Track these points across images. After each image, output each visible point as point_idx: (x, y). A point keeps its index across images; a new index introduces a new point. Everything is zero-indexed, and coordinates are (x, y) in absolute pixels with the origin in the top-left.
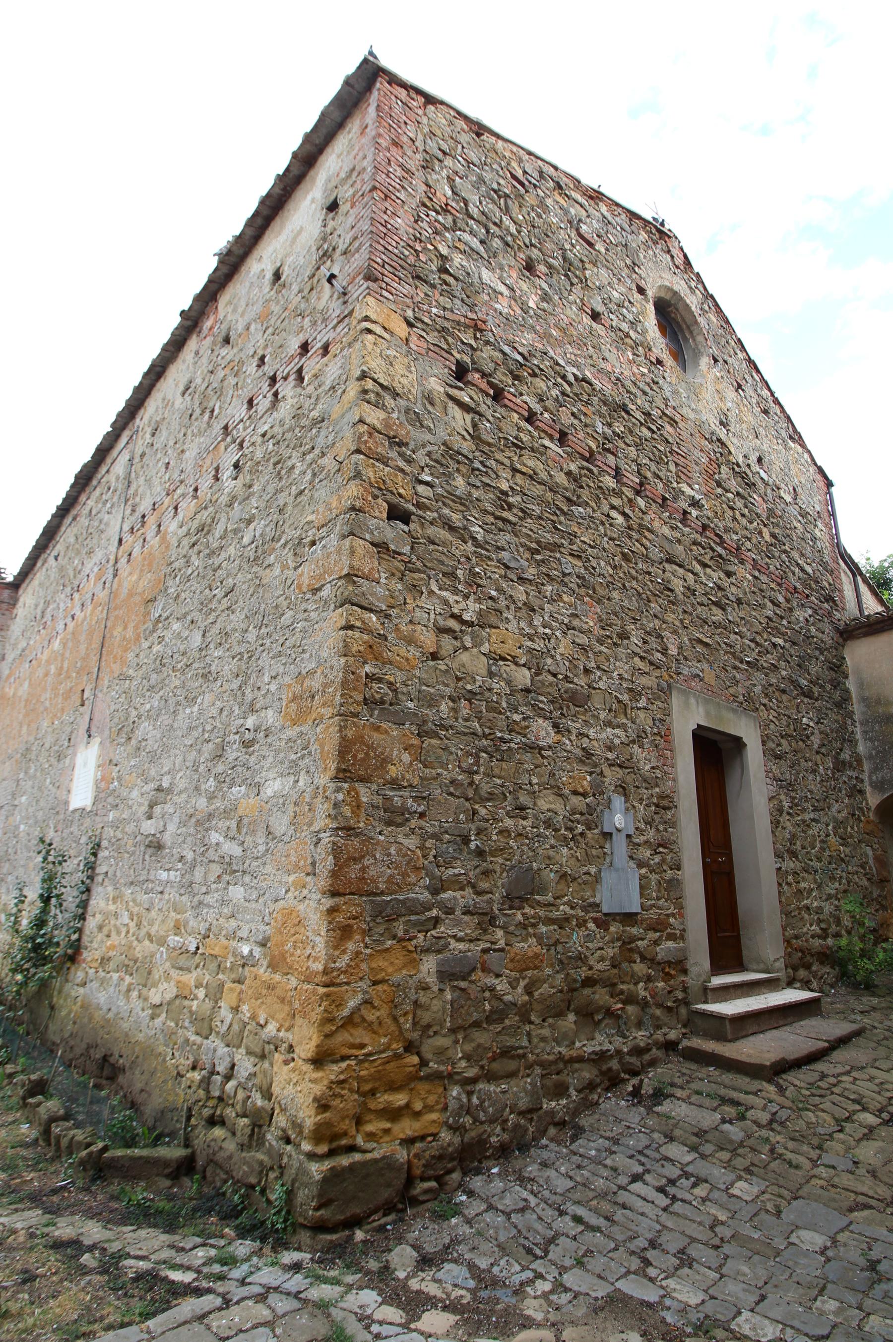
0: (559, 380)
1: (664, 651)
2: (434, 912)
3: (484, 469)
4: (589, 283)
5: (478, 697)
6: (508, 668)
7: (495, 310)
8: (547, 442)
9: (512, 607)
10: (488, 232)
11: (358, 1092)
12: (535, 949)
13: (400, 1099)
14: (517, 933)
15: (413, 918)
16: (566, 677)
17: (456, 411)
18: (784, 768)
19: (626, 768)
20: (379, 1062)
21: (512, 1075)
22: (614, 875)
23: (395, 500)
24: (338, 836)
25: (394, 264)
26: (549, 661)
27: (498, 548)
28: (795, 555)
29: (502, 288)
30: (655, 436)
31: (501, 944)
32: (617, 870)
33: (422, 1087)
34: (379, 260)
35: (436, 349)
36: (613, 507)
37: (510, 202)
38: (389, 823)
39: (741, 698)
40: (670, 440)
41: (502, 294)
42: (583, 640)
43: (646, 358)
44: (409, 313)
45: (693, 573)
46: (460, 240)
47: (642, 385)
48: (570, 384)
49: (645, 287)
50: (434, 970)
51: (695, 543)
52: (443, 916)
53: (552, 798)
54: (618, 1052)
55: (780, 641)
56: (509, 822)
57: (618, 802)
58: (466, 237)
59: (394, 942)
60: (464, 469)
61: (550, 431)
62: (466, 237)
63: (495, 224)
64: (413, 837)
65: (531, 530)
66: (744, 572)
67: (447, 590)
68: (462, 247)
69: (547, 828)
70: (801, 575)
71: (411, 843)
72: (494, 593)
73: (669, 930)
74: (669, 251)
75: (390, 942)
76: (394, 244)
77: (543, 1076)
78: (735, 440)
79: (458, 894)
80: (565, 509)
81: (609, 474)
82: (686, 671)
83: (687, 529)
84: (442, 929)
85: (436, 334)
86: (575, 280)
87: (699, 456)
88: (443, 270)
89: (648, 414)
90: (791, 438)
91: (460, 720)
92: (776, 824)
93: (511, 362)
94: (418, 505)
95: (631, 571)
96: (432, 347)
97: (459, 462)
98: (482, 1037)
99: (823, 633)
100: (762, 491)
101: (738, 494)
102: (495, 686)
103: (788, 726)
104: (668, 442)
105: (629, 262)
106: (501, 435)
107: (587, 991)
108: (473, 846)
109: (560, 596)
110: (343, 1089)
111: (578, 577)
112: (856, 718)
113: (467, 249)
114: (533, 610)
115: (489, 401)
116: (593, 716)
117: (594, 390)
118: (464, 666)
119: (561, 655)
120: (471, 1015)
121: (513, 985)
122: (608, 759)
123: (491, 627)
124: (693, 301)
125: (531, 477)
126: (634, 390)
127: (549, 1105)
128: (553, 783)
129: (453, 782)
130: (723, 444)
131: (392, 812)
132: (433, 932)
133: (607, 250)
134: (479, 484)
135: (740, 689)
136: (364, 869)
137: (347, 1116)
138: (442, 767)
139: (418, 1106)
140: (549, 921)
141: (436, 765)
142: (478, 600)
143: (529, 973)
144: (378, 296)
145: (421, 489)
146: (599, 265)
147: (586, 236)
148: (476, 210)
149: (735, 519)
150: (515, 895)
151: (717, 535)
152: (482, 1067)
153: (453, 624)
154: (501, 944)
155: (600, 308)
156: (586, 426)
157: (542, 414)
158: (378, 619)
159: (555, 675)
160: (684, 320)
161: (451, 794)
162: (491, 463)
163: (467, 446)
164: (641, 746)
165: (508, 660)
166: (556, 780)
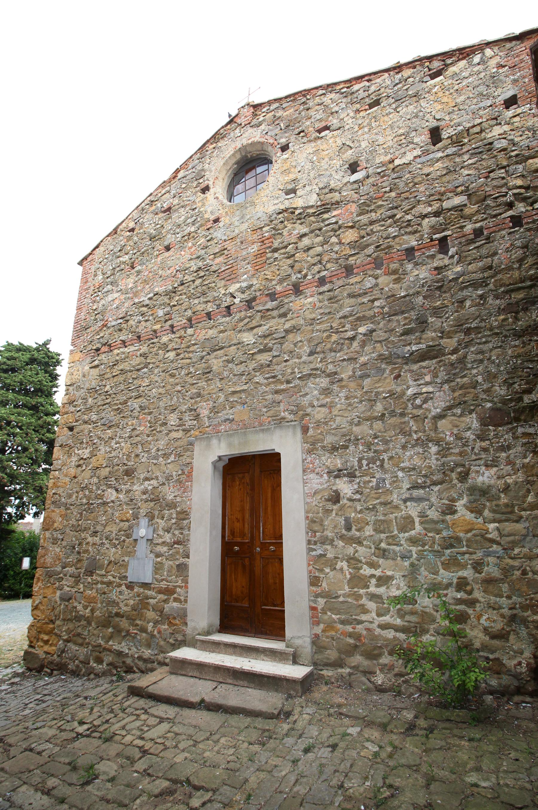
22: (136, 561)
31: (82, 590)
32: (138, 559)
38: (53, 544)
57: (144, 522)
71: (58, 550)
73: (175, 596)
79: (70, 569)
98: (71, 626)
107: (117, 619)
121: (85, 607)
127: (93, 664)
136: (45, 560)
140: (103, 583)
160: (259, 151)
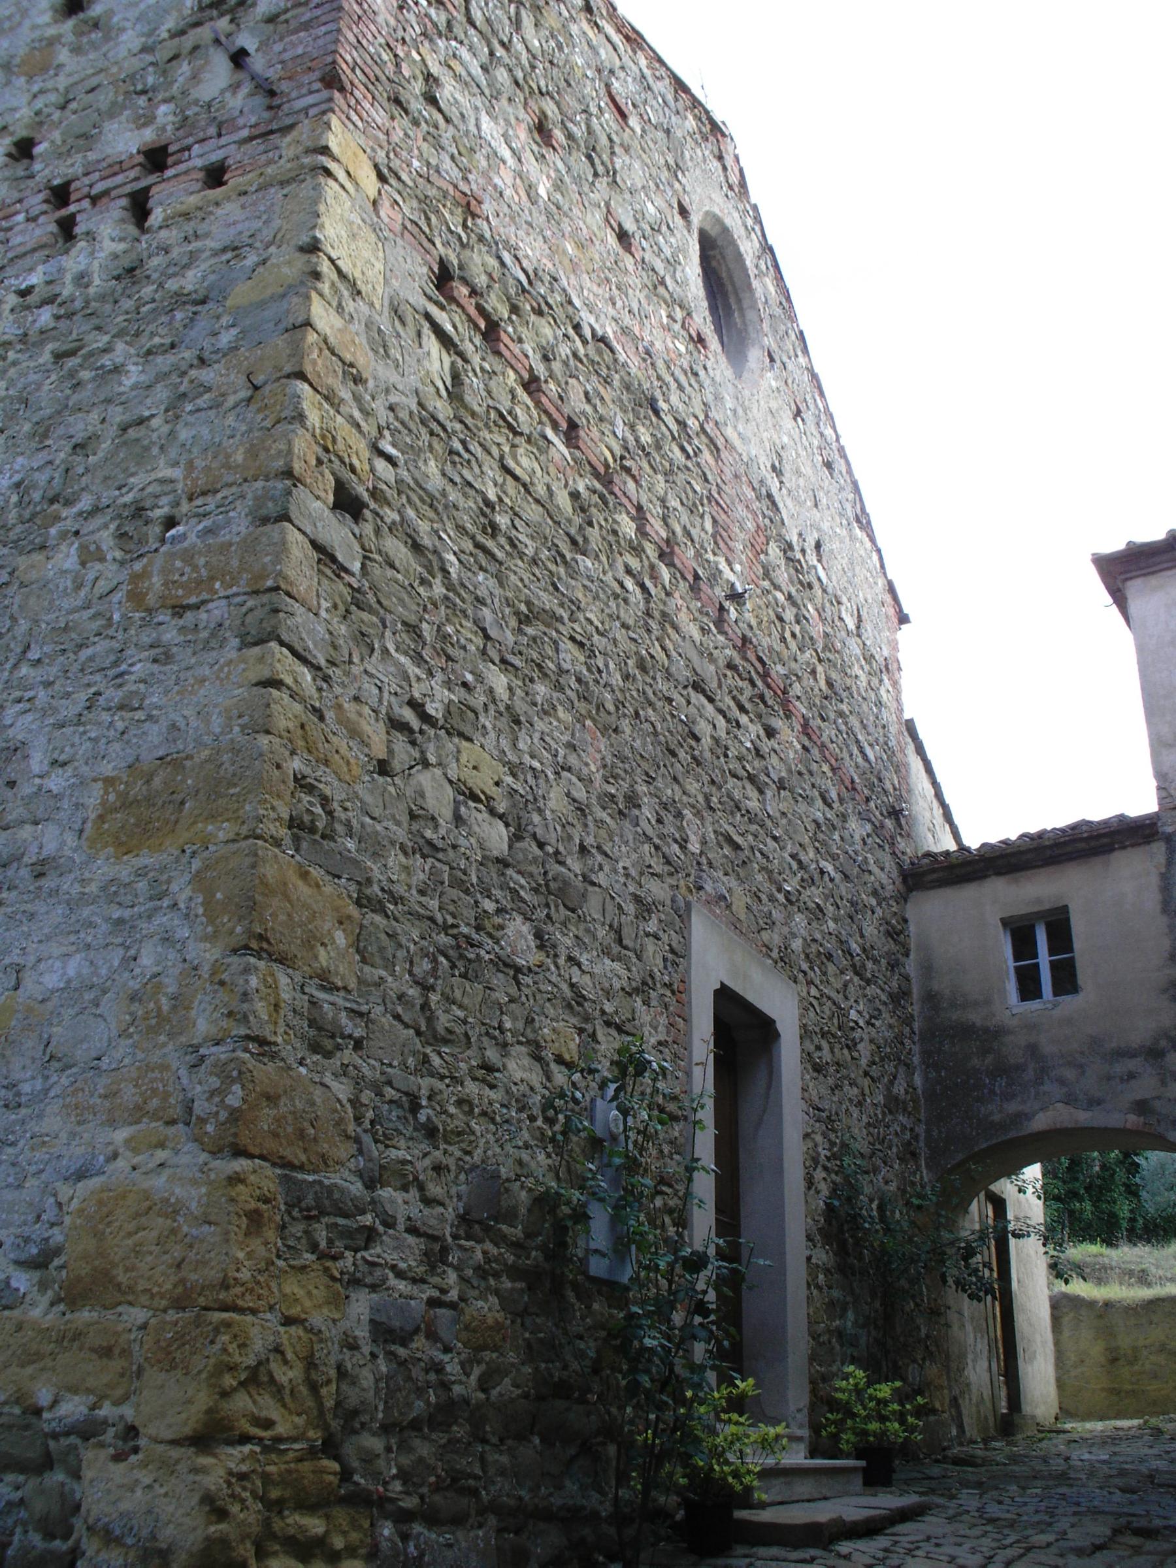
0: (571, 332)
1: (683, 844)
2: (367, 1219)
3: (466, 456)
4: (618, 179)
5: (440, 855)
6: (477, 816)
7: (495, 187)
8: (550, 433)
9: (492, 707)
10: (492, 54)
11: (262, 1499)
12: (497, 1315)
13: (315, 1525)
14: (475, 1284)
15: (341, 1221)
16: (557, 853)
17: (432, 343)
18: (824, 1091)
19: (628, 1034)
20: (291, 1455)
21: (457, 1521)
23: (346, 475)
24: (246, 1050)
25: (367, 70)
26: (536, 818)
27: (477, 599)
28: (854, 721)
29: (506, 153)
30: (689, 464)
31: (453, 1295)
33: (341, 1515)
34: (348, 58)
35: (415, 230)
36: (629, 571)
37: (523, 12)
38: (315, 1048)
39: (775, 955)
40: (710, 477)
41: (504, 162)
42: (580, 793)
43: (683, 326)
44: (381, 156)
45: (725, 717)
46: (454, 56)
47: (678, 372)
48: (585, 342)
49: (689, 208)
50: (365, 1318)
51: (731, 666)
52: (381, 1229)
53: (526, 1061)
54: (595, 1514)
55: (830, 868)
56: (472, 1088)
58: (464, 53)
59: (314, 1257)
60: (437, 446)
61: (556, 415)
62: (464, 53)
63: (502, 44)
64: (345, 1080)
65: (522, 580)
66: (788, 734)
67: (406, 653)
68: (459, 69)
69: (520, 1110)
70: (860, 760)
71: (342, 1090)
72: (469, 677)
74: (720, 158)
75: (308, 1256)
76: (370, 37)
77: (500, 1531)
78: (789, 502)
80: (568, 556)
81: (628, 513)
82: (708, 887)
83: (721, 638)
84: (378, 1250)
85: (415, 204)
86: (600, 169)
87: (745, 521)
88: (432, 100)
89: (682, 424)
90: (858, 521)
91: (414, 892)
92: (810, 1182)
93: (511, 281)
94: (374, 493)
95: (647, 689)
96: (409, 226)
97: (432, 433)
99: (882, 869)
100: (818, 601)
101: (790, 597)
102: (462, 841)
103: (831, 1019)
104: (706, 480)
105: (671, 162)
106: (491, 402)
108: (422, 1118)
109: (554, 708)
110: (244, 1489)
111: (579, 680)
112: (916, 1026)
113: (464, 73)
114: (517, 722)
115: (478, 340)
116: (588, 931)
117: (616, 360)
118: (423, 796)
119: (553, 811)
120: (410, 1405)
122: (603, 1012)
123: (461, 735)
124: (748, 248)
125: (524, 485)
126: (668, 379)
128: (531, 1036)
129: (401, 997)
130: (774, 503)
131: (320, 1029)
132: (366, 1254)
133: (643, 131)
134: (458, 479)
135: (776, 937)
137: (248, 1536)
138: (386, 968)
139: (338, 1543)
141: (378, 960)
142: (448, 684)
143: (487, 1355)
144: (343, 117)
145: (381, 465)
146: (632, 152)
147: (618, 98)
148: (479, 13)
149: (783, 639)
150: (474, 1215)
151: (760, 659)
152: (422, 1497)
153: (408, 715)
154: (453, 1295)
155: (630, 226)
156: (601, 419)
157: (546, 382)
158: (314, 680)
159: (541, 845)
160: (731, 277)
161: (397, 1017)
162: (474, 447)
163: (442, 408)
164: (647, 1003)
165: (480, 801)
166: (534, 1031)
